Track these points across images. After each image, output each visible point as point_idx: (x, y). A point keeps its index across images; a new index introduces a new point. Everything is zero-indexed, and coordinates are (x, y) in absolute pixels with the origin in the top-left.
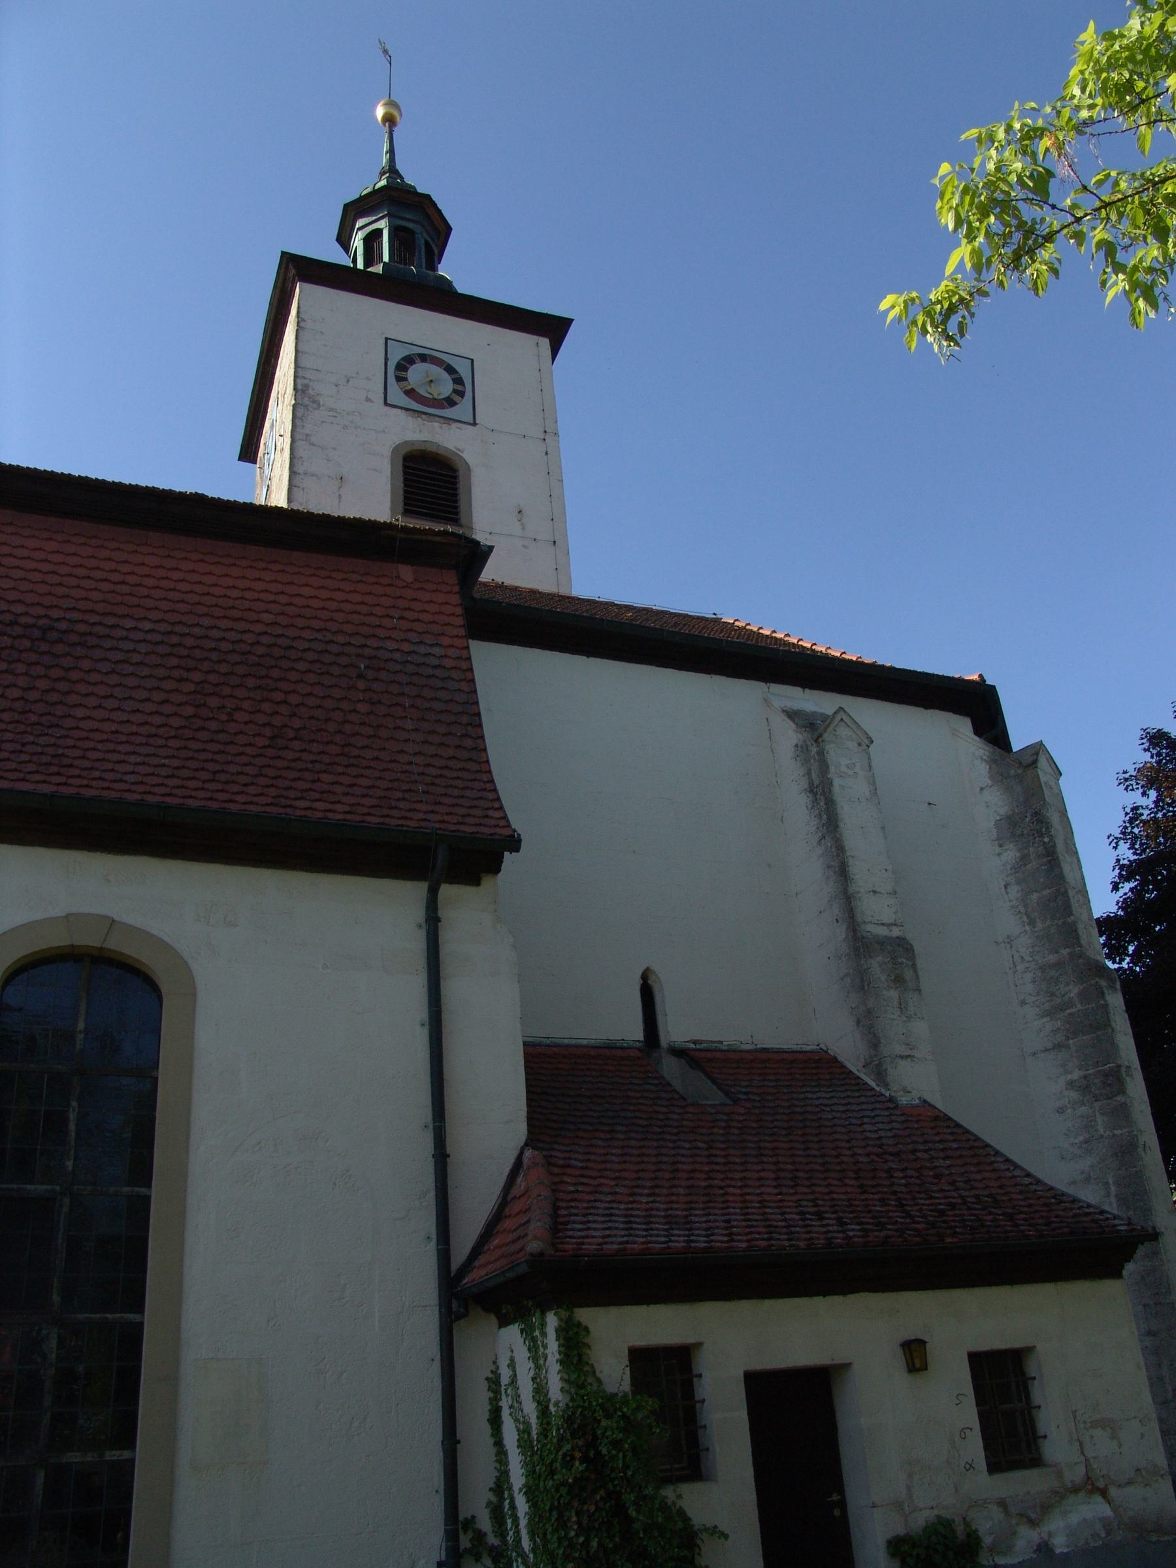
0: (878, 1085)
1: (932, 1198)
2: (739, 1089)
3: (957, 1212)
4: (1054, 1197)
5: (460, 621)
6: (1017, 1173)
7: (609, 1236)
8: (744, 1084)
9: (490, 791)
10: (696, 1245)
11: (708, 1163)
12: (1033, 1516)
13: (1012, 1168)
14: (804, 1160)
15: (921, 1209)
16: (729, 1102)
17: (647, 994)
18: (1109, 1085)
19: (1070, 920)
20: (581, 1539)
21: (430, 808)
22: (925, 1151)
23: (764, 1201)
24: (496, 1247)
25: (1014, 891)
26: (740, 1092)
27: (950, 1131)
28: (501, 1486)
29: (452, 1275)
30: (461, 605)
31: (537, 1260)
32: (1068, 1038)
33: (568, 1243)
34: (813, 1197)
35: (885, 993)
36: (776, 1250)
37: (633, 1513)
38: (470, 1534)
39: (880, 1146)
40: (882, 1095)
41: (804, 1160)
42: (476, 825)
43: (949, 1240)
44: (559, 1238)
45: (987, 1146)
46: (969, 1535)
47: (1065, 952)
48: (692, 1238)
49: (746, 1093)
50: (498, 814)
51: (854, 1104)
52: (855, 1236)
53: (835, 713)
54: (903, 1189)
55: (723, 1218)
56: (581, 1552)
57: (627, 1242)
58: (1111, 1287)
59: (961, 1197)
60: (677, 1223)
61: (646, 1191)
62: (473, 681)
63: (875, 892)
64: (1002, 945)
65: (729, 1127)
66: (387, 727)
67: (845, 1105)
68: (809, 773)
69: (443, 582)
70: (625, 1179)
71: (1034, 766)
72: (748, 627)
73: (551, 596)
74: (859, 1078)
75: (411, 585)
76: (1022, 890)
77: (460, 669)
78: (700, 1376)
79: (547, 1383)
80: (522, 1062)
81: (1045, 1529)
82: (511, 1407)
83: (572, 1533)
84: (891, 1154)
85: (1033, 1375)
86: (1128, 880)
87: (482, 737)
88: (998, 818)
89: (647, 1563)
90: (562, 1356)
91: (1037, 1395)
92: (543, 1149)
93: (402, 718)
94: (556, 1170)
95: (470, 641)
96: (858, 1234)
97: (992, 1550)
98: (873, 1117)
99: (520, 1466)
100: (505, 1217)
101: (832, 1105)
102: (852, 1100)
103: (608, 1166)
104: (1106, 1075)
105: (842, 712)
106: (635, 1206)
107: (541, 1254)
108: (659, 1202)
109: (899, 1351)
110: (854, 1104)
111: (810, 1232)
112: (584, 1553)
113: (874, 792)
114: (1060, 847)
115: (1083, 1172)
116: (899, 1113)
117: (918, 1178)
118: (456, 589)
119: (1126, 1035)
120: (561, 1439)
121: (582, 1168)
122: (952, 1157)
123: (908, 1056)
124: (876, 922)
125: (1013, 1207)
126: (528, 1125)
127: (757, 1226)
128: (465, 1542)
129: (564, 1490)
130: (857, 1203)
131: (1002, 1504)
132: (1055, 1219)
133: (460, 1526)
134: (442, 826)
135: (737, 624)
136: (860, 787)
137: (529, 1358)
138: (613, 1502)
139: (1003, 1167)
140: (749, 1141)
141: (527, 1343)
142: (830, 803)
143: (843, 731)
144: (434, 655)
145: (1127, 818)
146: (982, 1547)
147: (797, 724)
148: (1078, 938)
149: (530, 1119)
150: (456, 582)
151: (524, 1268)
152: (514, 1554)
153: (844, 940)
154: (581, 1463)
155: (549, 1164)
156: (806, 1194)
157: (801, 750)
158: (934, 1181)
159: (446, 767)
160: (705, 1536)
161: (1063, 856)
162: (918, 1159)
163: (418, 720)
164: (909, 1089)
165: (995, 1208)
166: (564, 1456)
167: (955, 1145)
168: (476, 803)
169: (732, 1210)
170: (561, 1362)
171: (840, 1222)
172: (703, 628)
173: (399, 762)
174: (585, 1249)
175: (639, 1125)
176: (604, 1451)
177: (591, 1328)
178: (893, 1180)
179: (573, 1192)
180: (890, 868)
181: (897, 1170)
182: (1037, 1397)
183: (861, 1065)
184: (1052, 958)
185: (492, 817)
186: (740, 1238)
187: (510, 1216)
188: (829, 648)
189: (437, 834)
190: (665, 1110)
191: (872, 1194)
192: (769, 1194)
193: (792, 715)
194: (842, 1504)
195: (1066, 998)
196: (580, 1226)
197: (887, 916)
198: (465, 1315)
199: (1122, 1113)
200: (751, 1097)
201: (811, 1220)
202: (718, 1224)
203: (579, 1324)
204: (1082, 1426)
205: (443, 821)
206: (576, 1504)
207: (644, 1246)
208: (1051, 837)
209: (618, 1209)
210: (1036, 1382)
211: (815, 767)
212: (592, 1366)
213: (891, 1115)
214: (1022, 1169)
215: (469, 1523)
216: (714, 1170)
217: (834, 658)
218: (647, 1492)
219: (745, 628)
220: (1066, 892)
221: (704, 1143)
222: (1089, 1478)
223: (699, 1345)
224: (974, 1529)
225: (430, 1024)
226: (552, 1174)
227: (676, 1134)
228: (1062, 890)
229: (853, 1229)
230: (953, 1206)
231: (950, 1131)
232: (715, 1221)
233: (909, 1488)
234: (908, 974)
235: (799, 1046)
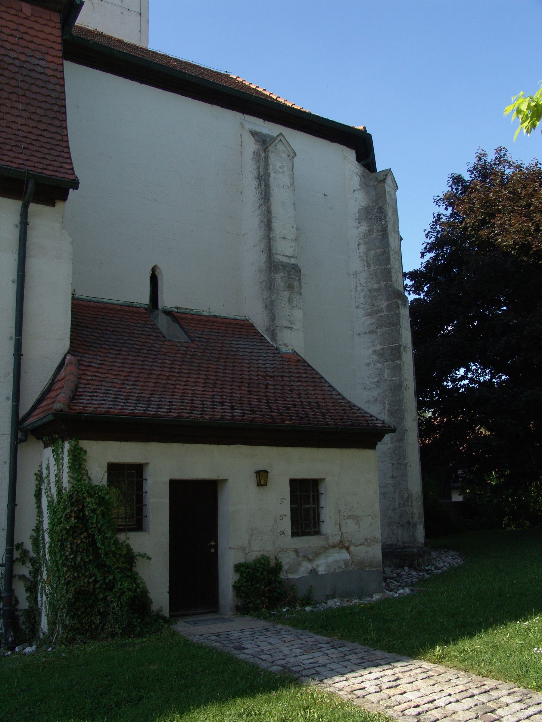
0: (271, 341)
1: (286, 400)
2: (196, 335)
3: (296, 409)
4: (349, 407)
5: (59, 47)
6: (334, 393)
7: (103, 404)
8: (200, 333)
9: (66, 153)
10: (150, 412)
11: (169, 372)
12: (311, 557)
13: (332, 390)
14: (222, 375)
15: (278, 406)
16: (190, 341)
17: (154, 280)
18: (394, 355)
19: (388, 267)
20: (72, 556)
21: (27, 158)
22: (289, 377)
23: (195, 394)
24: (46, 406)
25: (362, 248)
26: (196, 337)
27: (304, 368)
28: (38, 529)
29: (20, 419)
30: (61, 36)
31: (59, 415)
32: (377, 328)
33: (78, 406)
34: (222, 394)
35: (281, 292)
36: (193, 419)
37: (99, 545)
38: (20, 551)
39: (265, 372)
40: (273, 346)
41: (222, 375)
42: (54, 171)
43: (287, 422)
44: (73, 403)
45: (322, 377)
46: (277, 564)
47: (383, 283)
48: (149, 409)
49: (199, 338)
50: (68, 167)
51: (256, 349)
52: (237, 416)
53: (277, 136)
54: (272, 395)
55: (169, 400)
56: (71, 562)
57: (112, 408)
58: (368, 453)
59: (301, 402)
60: (143, 401)
61: (131, 383)
62: (64, 85)
63: (284, 238)
64: (352, 276)
65: (186, 354)
66: (6, 106)
67: (252, 349)
68: (258, 168)
69: (51, 20)
70: (121, 375)
71: (383, 182)
72: (244, 82)
73: (136, 48)
74: (263, 336)
75: (29, 18)
76: (366, 248)
77: (56, 77)
78: (146, 480)
79: (62, 478)
80: (70, 308)
81: (315, 563)
82: (45, 489)
83: (68, 553)
84: (270, 376)
85: (322, 492)
86: (429, 251)
87: (65, 120)
88: (360, 208)
89: (106, 569)
90: (70, 464)
91: (323, 502)
92: (77, 356)
93: (16, 101)
94: (83, 368)
95: (64, 61)
96: (240, 415)
97: (287, 572)
98: (265, 357)
99: (48, 519)
100: (52, 390)
101: (245, 348)
102: (256, 347)
103: (113, 368)
104: (393, 349)
105: (281, 136)
106: (122, 390)
107: (62, 411)
108: (136, 389)
109: (254, 476)
110: (256, 349)
111: (214, 411)
112: (73, 563)
113: (293, 184)
114: (390, 227)
115: (374, 397)
116: (280, 356)
117: (281, 390)
118: (59, 26)
119: (407, 330)
120: (65, 509)
121: (98, 368)
122: (302, 381)
123: (290, 327)
124: (283, 254)
125: (327, 410)
126: (71, 342)
127: (186, 406)
128: (17, 554)
129: (64, 532)
130: (245, 399)
131: (296, 551)
132: (346, 417)
133: (15, 547)
134: (33, 169)
135: (238, 79)
136: (285, 179)
137: (55, 465)
138: (91, 539)
139: (327, 389)
140: (195, 362)
141: (55, 457)
142: (267, 186)
143: (280, 147)
144: (41, 66)
145: (434, 220)
146: (282, 570)
147: (256, 140)
148: (390, 277)
149: (72, 338)
150: (59, 21)
151: (51, 418)
152: (42, 562)
153: (264, 262)
154: (75, 519)
155: (80, 364)
156: (219, 392)
157: (257, 154)
158: (289, 392)
159: (41, 135)
160: (139, 558)
161: (390, 232)
162: (283, 380)
163: (27, 104)
164: (288, 344)
165: (317, 409)
166: (66, 515)
167: (305, 375)
168: (56, 158)
169: (176, 397)
170: (70, 467)
171: (232, 408)
172: (217, 78)
173: (12, 128)
174: (87, 410)
175: (136, 349)
176: (87, 514)
177: (88, 450)
178: (267, 389)
179: (89, 380)
180: (295, 226)
181: (271, 385)
182: (322, 503)
183: (264, 329)
184: (376, 286)
185: (65, 168)
186: (175, 411)
187: (54, 390)
188: (286, 100)
189: (28, 173)
190: (152, 342)
191: (255, 395)
192: (198, 390)
193: (254, 134)
194: (216, 547)
195: (380, 308)
196: (88, 398)
197: (289, 252)
198: (25, 440)
199: (398, 369)
200: (202, 339)
201: (217, 405)
202: (165, 403)
203: (81, 449)
204: (342, 517)
205: (34, 167)
206: (70, 539)
207: (120, 411)
208: (386, 222)
209: (112, 390)
210: (323, 496)
211: (262, 164)
212: (87, 471)
213: (275, 357)
214: (337, 391)
215: (19, 546)
216: (171, 376)
217: (289, 107)
218: (107, 535)
219: (242, 82)
220: (389, 251)
221: (170, 361)
222: (341, 542)
223: (147, 464)
224: (280, 561)
225: (18, 281)
226: (80, 369)
227: (155, 355)
228: (387, 251)
229: (238, 413)
230: (295, 406)
231: (304, 368)
232: (165, 401)
233: (250, 542)
234: (296, 284)
235: (234, 316)
